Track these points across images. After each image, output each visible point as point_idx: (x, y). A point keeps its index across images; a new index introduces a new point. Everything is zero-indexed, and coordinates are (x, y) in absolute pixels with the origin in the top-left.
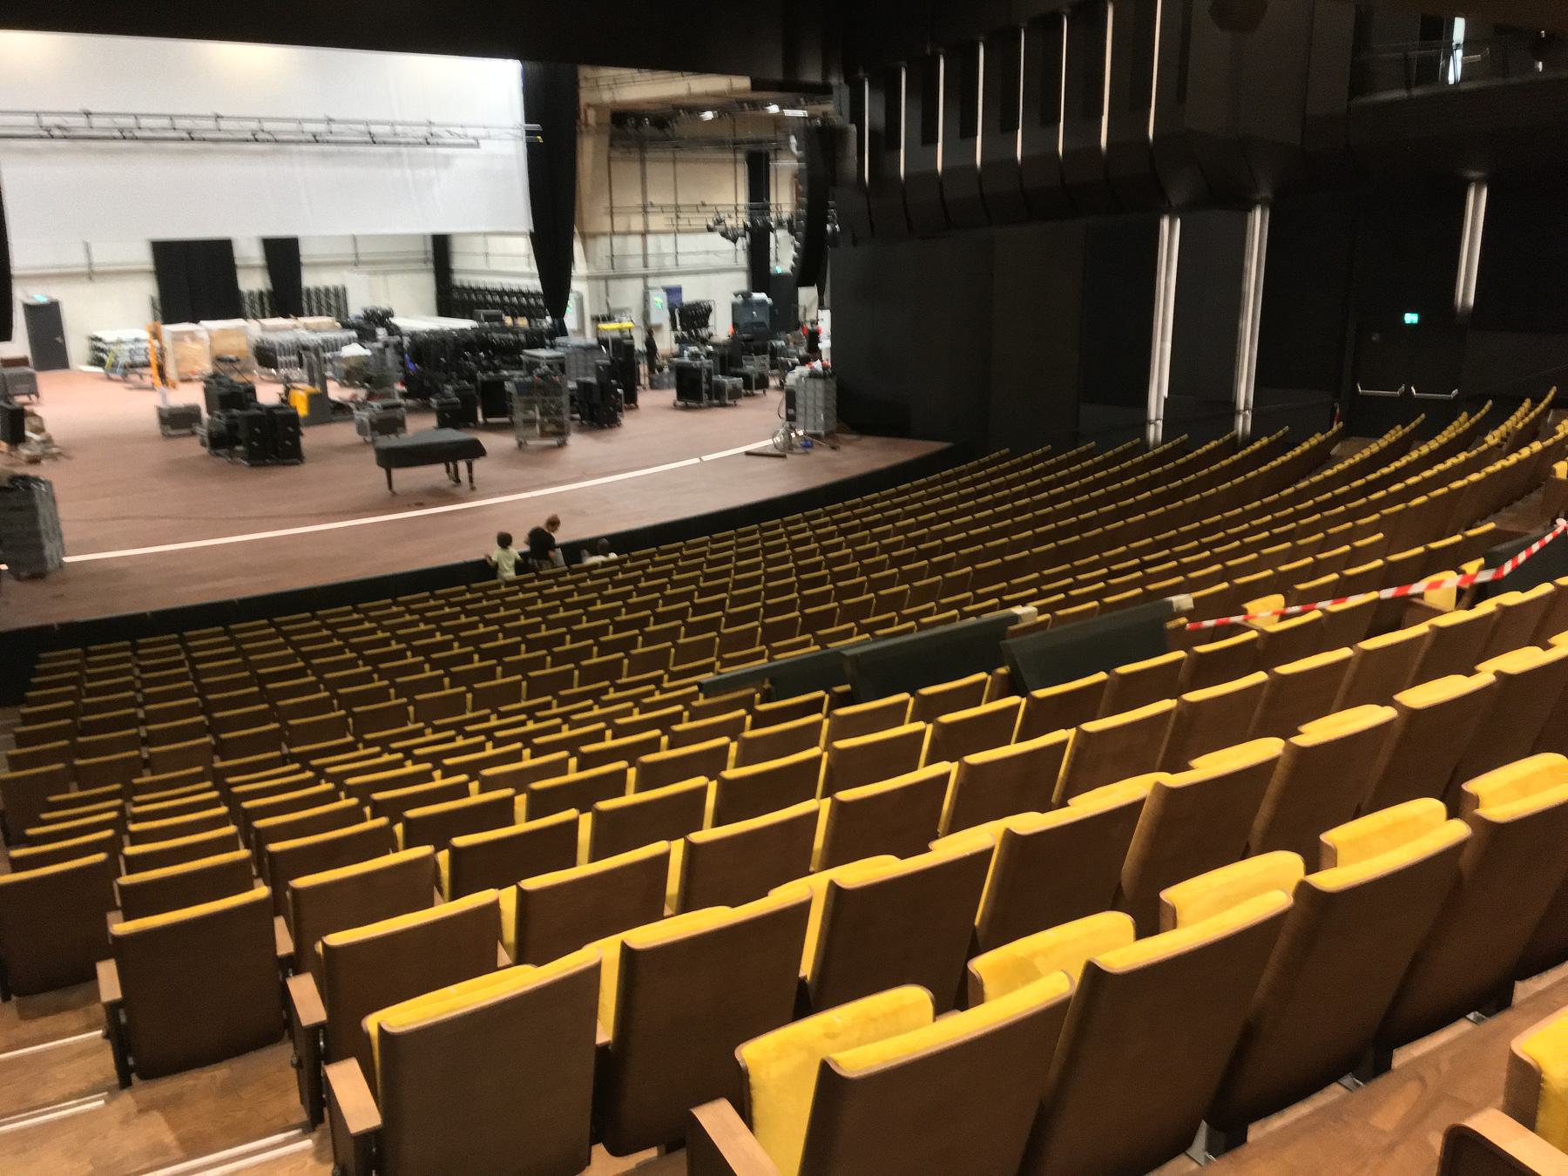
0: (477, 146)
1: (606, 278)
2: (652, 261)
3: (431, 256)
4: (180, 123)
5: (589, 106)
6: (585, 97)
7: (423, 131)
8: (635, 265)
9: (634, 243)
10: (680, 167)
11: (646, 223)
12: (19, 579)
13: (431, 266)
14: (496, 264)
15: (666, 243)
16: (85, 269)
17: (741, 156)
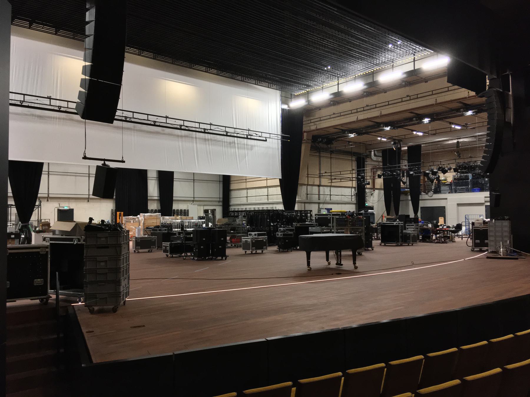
0: (266, 141)
1: (305, 203)
2: (321, 196)
3: (221, 200)
4: (150, 118)
5: (305, 132)
6: (305, 128)
7: (246, 133)
8: (315, 198)
9: (315, 189)
10: (333, 161)
11: (320, 181)
12: (92, 312)
13: (221, 204)
14: (251, 200)
15: (327, 190)
16: (46, 196)
17: (354, 159)
